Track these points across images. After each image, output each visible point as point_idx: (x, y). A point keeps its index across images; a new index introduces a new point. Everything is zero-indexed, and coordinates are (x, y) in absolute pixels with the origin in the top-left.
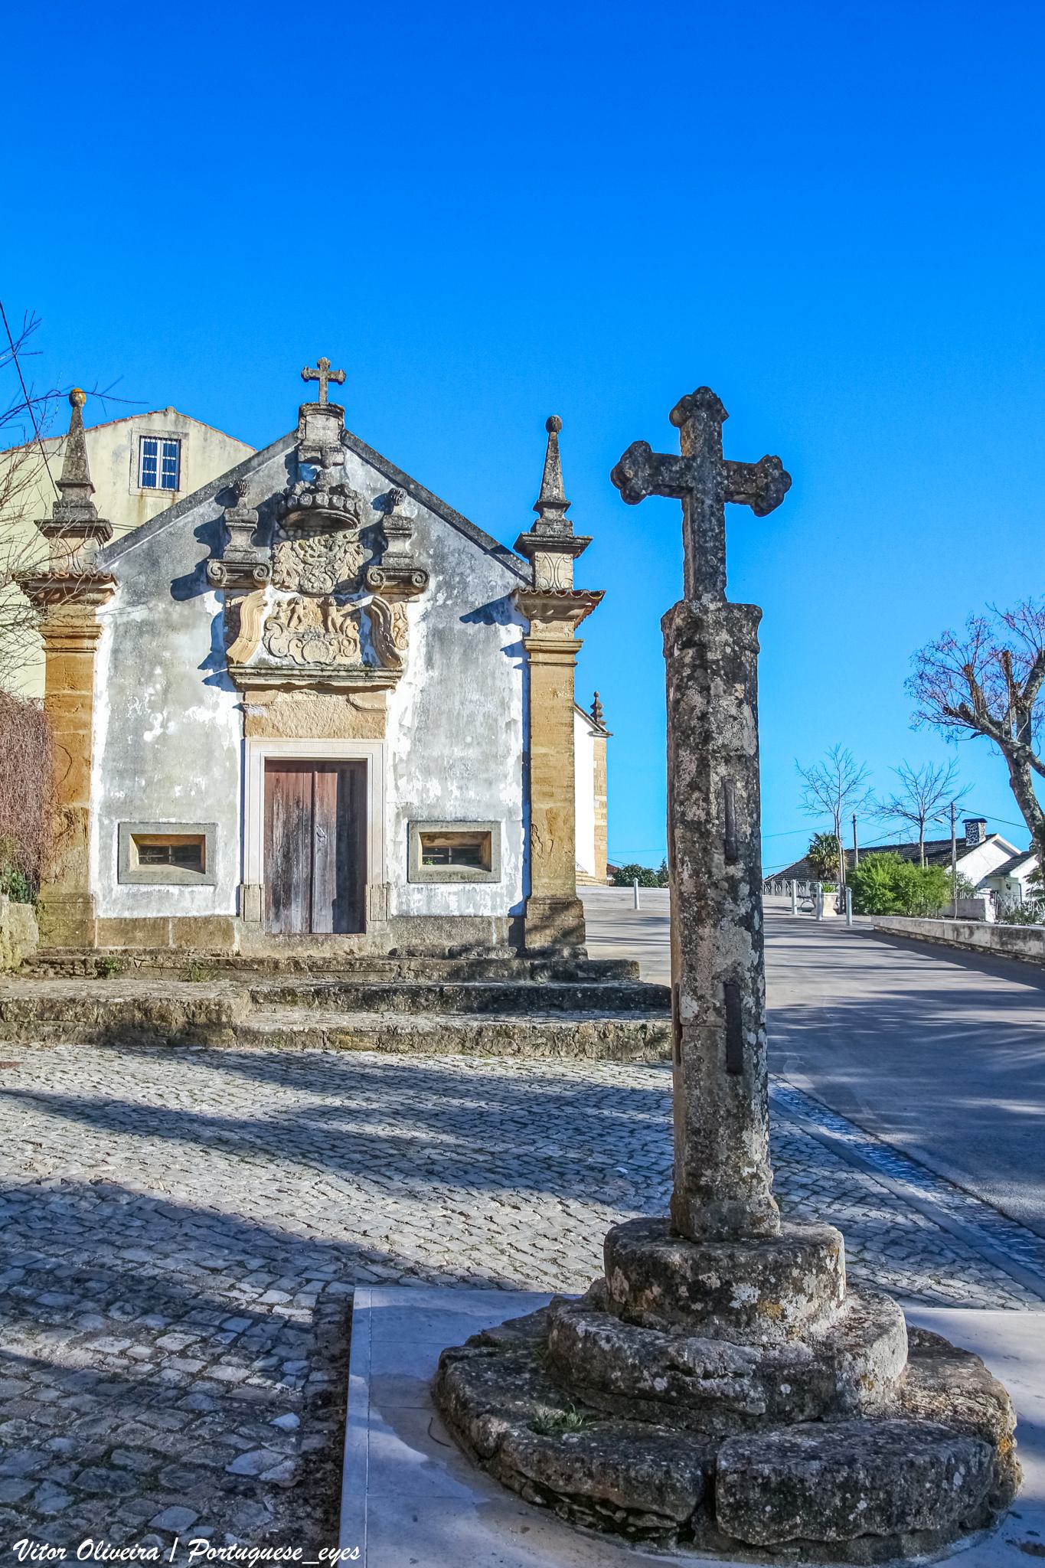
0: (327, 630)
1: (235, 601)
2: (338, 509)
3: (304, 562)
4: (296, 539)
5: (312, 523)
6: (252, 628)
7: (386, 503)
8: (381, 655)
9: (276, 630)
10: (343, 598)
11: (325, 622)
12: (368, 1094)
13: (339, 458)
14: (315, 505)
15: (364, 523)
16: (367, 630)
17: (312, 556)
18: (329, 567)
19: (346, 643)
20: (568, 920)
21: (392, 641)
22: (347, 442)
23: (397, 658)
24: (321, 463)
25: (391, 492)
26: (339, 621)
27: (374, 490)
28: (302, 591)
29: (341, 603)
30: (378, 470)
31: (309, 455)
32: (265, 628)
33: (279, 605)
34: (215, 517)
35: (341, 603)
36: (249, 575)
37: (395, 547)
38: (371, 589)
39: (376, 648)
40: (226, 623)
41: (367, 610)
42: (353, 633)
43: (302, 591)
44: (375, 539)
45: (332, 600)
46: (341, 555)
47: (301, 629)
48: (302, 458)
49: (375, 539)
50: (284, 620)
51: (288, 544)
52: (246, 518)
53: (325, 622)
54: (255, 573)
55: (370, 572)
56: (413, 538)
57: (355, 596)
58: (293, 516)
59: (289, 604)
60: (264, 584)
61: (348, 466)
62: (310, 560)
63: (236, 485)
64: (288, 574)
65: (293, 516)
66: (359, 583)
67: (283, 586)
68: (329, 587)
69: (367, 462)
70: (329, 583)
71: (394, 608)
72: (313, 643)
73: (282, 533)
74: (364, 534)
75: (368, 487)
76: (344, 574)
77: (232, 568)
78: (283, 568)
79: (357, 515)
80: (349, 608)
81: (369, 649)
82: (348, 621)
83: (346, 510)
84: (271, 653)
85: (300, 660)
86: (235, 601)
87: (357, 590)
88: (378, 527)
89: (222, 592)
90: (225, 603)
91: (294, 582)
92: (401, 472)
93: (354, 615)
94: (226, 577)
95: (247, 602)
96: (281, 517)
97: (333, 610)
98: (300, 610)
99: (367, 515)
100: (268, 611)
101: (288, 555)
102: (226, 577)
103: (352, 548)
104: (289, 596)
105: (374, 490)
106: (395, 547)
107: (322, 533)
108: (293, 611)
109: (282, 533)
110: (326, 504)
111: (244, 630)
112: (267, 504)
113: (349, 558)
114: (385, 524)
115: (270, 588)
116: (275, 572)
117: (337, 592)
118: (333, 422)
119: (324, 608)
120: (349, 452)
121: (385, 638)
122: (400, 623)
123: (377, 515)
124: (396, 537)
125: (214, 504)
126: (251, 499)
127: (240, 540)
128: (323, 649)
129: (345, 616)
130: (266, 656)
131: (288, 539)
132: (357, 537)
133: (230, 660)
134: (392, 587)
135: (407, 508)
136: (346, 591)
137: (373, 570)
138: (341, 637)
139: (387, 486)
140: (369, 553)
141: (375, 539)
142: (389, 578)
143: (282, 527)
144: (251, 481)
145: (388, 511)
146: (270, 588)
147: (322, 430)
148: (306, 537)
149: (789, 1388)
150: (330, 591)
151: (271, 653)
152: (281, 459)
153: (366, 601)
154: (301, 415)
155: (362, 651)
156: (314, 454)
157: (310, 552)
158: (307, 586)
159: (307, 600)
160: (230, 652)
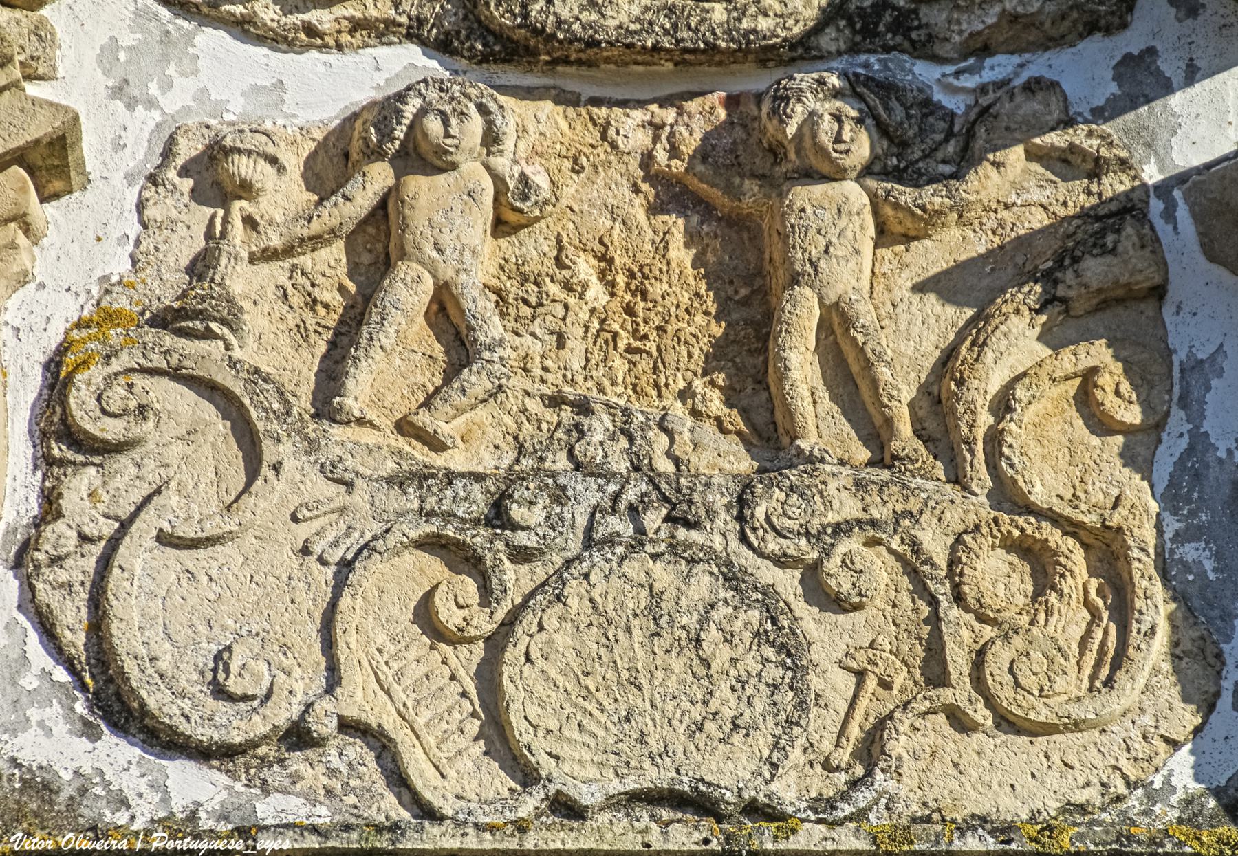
0: (770, 436)
9: (182, 445)
12: (518, 737)
19: (996, 574)
20: (758, 282)
26: (906, 342)
29: (920, 150)
33: (214, 175)
35: (920, 150)
42: (1061, 459)
45: (817, 107)
47: (476, 441)
50: (271, 342)
57: (1084, 69)
59: (333, 163)
72: (615, 584)
80: (1015, 192)
82: (1017, 342)
84: (114, 704)
97: (835, 226)
98: (451, 224)
108: (378, 244)
119: (733, 207)
128: (736, 652)
129: (964, 285)
149: (722, 375)
151: (114, 704)
159: (535, 126)
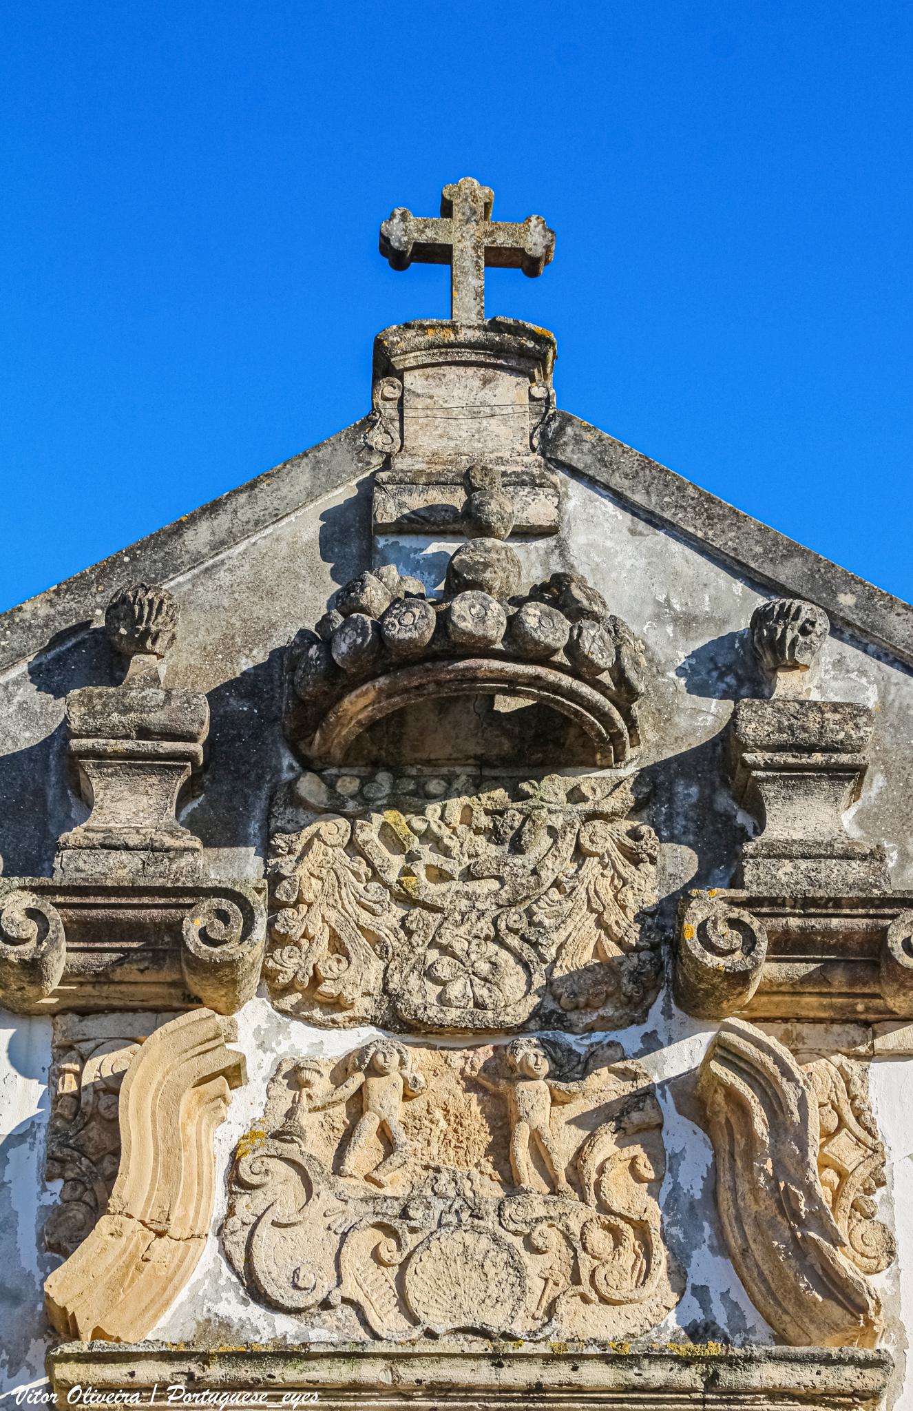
0: (511, 1183)
1: (96, 1069)
2: (543, 656)
3: (406, 899)
4: (367, 805)
5: (438, 747)
6: (169, 1172)
7: (743, 665)
8: (775, 1300)
9: (281, 1186)
10: (575, 1042)
11: (501, 1150)
13: (539, 510)
14: (449, 643)
15: (651, 746)
16: (692, 1180)
17: (441, 876)
18: (514, 917)
19: (599, 1239)
21: (820, 1220)
22: (568, 454)
23: (850, 1299)
24: (471, 522)
25: (760, 617)
26: (564, 1143)
27: (687, 622)
28: (399, 1021)
29: (569, 1068)
30: (702, 548)
31: (416, 501)
32: (236, 1183)
33: (295, 1078)
34: (28, 738)
36: (163, 944)
37: (796, 818)
38: (696, 998)
39: (739, 1260)
40: (54, 1165)
41: (693, 1095)
42: (626, 1194)
43: (399, 1021)
44: (711, 801)
45: (528, 1051)
46: (559, 866)
47: (396, 1183)
48: (387, 510)
49: (705, 805)
50: (316, 1144)
51: (334, 829)
52: (157, 718)
53: (501, 1150)
54: (192, 928)
55: (697, 913)
56: (876, 783)
57: (630, 1038)
58: (358, 706)
59: (341, 1073)
60: (224, 974)
61: (578, 539)
62: (431, 891)
63: (120, 609)
64: (338, 947)
65: (358, 706)
66: (658, 973)
67: (314, 1001)
68: (515, 997)
69: (654, 521)
70: (513, 981)
71: (818, 1078)
72: (450, 1242)
73: (309, 787)
74: (653, 789)
75: (663, 611)
76: (578, 944)
77: (94, 917)
78: (314, 922)
79: (625, 693)
80: (604, 1086)
81: (708, 1267)
82: (606, 1145)
83: (581, 666)
84: (255, 1292)
85: (388, 1321)
86: (96, 1069)
87: (636, 1010)
88: (722, 754)
89: (43, 1035)
90: (54, 1076)
91: (360, 980)
92: (793, 551)
93: (632, 1117)
94: (61, 960)
95: (148, 1069)
96: (311, 715)
97: (534, 1098)
98: (386, 1098)
99: (664, 718)
100: (248, 1106)
101: (331, 864)
102: (61, 960)
103: (604, 838)
104: (342, 1042)
105: (687, 622)
106: (796, 818)
107: (478, 785)
108: (358, 1104)
109: (309, 787)
110: (496, 632)
111: (135, 1183)
112: (248, 685)
113: (591, 868)
114: (749, 730)
115: (254, 1013)
116: (276, 940)
117: (546, 1019)
118: (510, 390)
119: (495, 1089)
120: (577, 492)
121: (785, 1204)
122: (845, 1150)
123: (705, 717)
124: (797, 778)
125: (28, 692)
126: (182, 670)
127: (130, 808)
128: (498, 1271)
129: (589, 1122)
130: (233, 1307)
131: (335, 808)
132: (623, 798)
133: (59, 1326)
134: (796, 988)
135: (825, 676)
136: (577, 1018)
137: (709, 907)
138: (579, 1214)
139: (736, 605)
140: (683, 860)
141: (711, 801)
142: (784, 946)
143: (307, 765)
144: (186, 603)
145: (723, 850)
146: (254, 1013)
147: (466, 418)
148: (412, 800)
150: (521, 1012)
152: (306, 527)
153: (684, 1055)
154: (384, 366)
155: (678, 1274)
156: (436, 497)
157: (429, 857)
158: (420, 997)
159: (419, 1058)
160: (66, 1285)
